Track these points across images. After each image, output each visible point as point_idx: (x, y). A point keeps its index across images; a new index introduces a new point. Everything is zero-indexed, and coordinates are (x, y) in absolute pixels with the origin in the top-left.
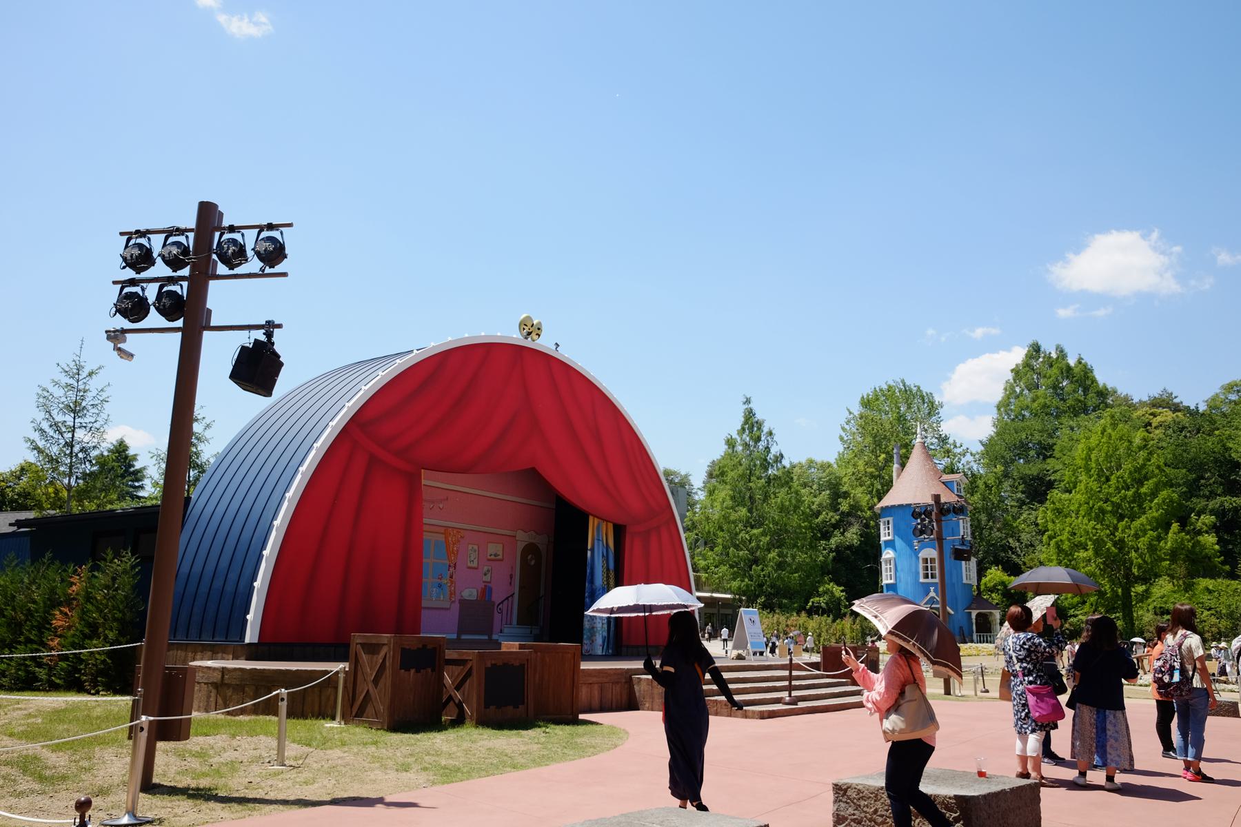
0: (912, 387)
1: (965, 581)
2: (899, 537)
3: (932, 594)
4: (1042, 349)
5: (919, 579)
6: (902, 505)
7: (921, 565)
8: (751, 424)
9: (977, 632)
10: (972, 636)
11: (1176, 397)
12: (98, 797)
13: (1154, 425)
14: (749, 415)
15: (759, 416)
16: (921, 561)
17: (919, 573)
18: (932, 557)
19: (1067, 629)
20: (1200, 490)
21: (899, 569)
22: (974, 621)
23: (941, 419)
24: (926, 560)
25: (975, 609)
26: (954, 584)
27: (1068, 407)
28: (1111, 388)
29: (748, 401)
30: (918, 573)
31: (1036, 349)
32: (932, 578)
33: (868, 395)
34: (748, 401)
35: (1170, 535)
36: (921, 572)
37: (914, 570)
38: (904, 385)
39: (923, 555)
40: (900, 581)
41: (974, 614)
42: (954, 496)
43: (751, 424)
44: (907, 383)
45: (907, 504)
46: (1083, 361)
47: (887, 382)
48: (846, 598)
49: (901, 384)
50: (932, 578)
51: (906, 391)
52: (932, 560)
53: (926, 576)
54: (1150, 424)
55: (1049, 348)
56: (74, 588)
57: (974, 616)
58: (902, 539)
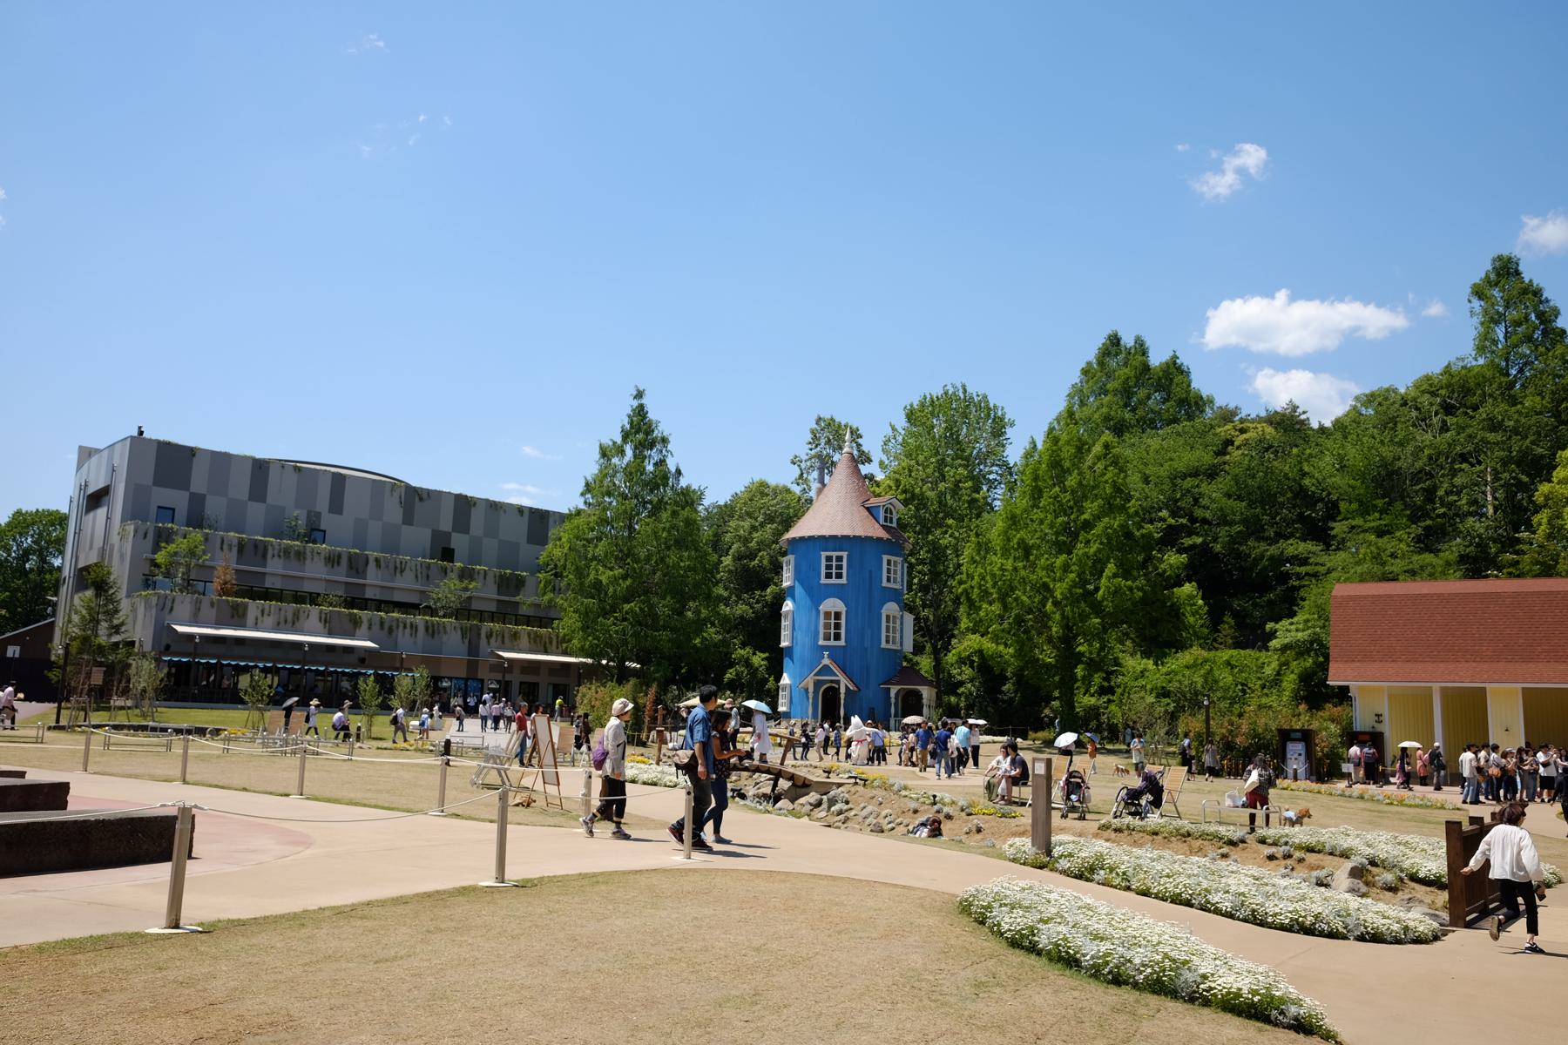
0: (975, 396)
1: (884, 645)
3: (826, 661)
4: (1122, 342)
6: (824, 536)
7: (822, 621)
8: (641, 431)
11: (1304, 413)
13: (1236, 444)
14: (641, 412)
15: (652, 415)
16: (822, 616)
19: (1046, 716)
22: (893, 700)
24: (827, 615)
25: (894, 684)
26: (866, 649)
29: (639, 395)
30: (817, 633)
31: (1115, 340)
32: (835, 639)
33: (911, 405)
34: (639, 395)
35: (1103, 580)
36: (822, 631)
37: (813, 629)
41: (894, 690)
42: (877, 525)
43: (641, 431)
45: (809, 537)
46: (1178, 361)
48: (767, 669)
49: (961, 390)
50: (835, 639)
51: (969, 401)
52: (838, 615)
53: (827, 638)
54: (1232, 443)
55: (1128, 340)
56: (1243, 727)
57: (893, 694)
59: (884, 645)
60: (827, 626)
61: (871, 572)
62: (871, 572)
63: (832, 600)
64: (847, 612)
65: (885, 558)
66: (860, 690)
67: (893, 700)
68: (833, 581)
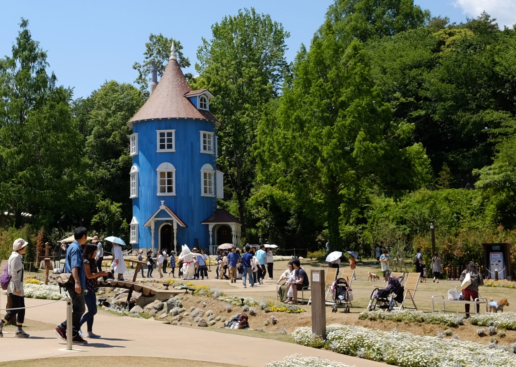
0: (261, 16)
2: (142, 152)
3: (163, 207)
5: (156, 193)
9: (212, 244)
10: (208, 248)
11: (494, 20)
12: (420, 327)
13: (447, 43)
14: (26, 36)
15: (34, 38)
17: (157, 187)
18: (169, 171)
19: (320, 240)
20: (469, 104)
21: (141, 182)
22: (211, 233)
23: (287, 47)
24: (162, 174)
26: (191, 197)
27: (376, 29)
28: (425, 11)
29: (24, 24)
30: (155, 187)
33: (217, 24)
34: (24, 24)
36: (159, 186)
37: (152, 184)
38: (254, 13)
39: (160, 169)
40: (141, 196)
41: (211, 226)
42: (195, 110)
44: (257, 12)
45: (148, 120)
47: (240, 10)
49: (251, 13)
52: (170, 174)
57: (210, 229)
58: (144, 155)
59: (203, 194)
60: (163, 182)
61: (192, 143)
62: (192, 143)
63: (165, 163)
64: (176, 172)
65: (202, 133)
66: (187, 227)
67: (211, 233)
68: (166, 150)
